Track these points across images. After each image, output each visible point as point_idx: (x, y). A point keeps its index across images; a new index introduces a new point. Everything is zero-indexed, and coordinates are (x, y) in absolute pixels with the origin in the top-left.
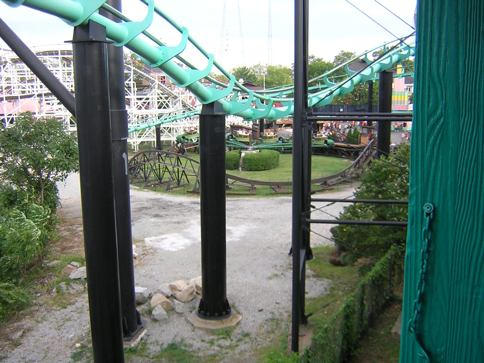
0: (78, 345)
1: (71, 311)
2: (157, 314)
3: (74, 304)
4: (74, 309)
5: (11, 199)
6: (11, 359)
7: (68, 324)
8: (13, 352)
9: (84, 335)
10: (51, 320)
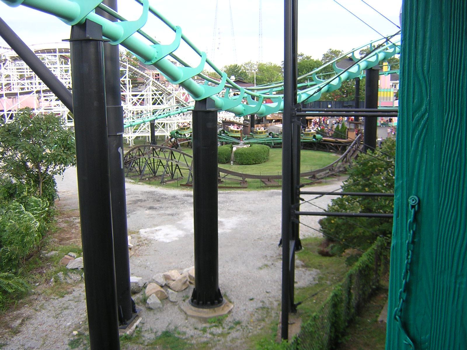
0: (75, 333)
1: (69, 300)
2: (151, 303)
3: (71, 294)
4: (71, 298)
5: (11, 191)
6: (10, 346)
7: (66, 312)
8: (12, 339)
9: (81, 323)
10: (50, 309)
